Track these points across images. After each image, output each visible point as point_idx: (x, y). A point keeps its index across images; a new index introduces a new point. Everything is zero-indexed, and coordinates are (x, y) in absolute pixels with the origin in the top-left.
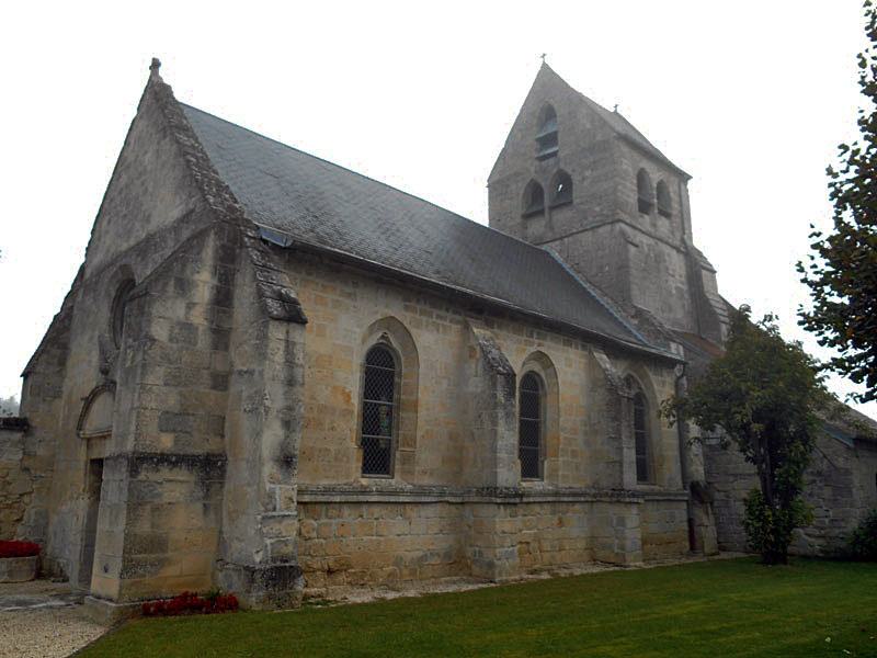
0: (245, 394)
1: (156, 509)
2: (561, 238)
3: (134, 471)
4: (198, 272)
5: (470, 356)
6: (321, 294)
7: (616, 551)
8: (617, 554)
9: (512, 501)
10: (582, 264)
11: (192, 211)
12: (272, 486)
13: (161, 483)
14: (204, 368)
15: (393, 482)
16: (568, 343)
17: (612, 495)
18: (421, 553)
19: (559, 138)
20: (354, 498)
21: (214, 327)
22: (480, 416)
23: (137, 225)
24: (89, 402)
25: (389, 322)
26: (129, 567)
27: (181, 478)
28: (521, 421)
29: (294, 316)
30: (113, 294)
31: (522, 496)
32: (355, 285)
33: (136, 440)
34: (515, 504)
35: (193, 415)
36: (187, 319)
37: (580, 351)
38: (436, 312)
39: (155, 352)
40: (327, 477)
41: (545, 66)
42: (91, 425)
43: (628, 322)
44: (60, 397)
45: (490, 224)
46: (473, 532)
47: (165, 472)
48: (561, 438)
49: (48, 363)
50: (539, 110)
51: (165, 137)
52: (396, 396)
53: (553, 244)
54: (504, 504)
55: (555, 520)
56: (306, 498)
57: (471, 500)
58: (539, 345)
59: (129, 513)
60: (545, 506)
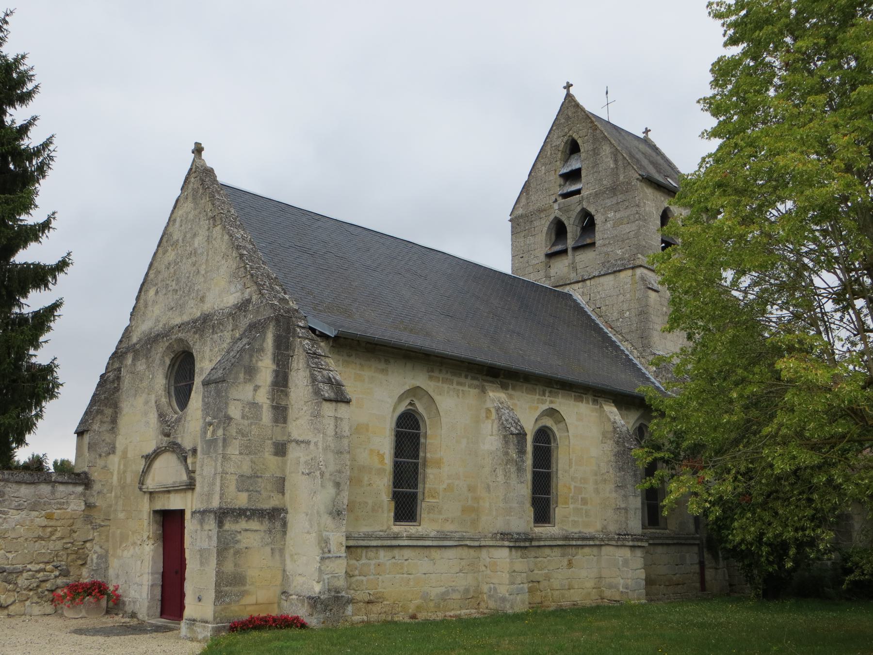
0: (302, 460)
1: (237, 553)
2: (584, 281)
3: (220, 524)
5: (487, 417)
6: (358, 372)
7: (621, 589)
9: (522, 544)
11: (249, 301)
13: (240, 532)
14: (268, 439)
15: (420, 528)
16: (579, 399)
18: (443, 589)
19: (583, 175)
20: (389, 543)
21: (274, 404)
23: (191, 303)
25: (415, 391)
28: (534, 472)
29: (341, 398)
31: (531, 540)
32: (387, 362)
33: (221, 498)
34: (526, 547)
35: (261, 477)
36: (254, 399)
37: (591, 406)
38: (455, 379)
39: (233, 430)
41: (569, 97)
42: (153, 480)
44: (114, 452)
45: (518, 254)
47: (243, 524)
48: (572, 487)
49: (102, 422)
51: (215, 226)
52: (421, 454)
53: (576, 286)
57: (487, 543)
58: (551, 402)
60: (555, 549)
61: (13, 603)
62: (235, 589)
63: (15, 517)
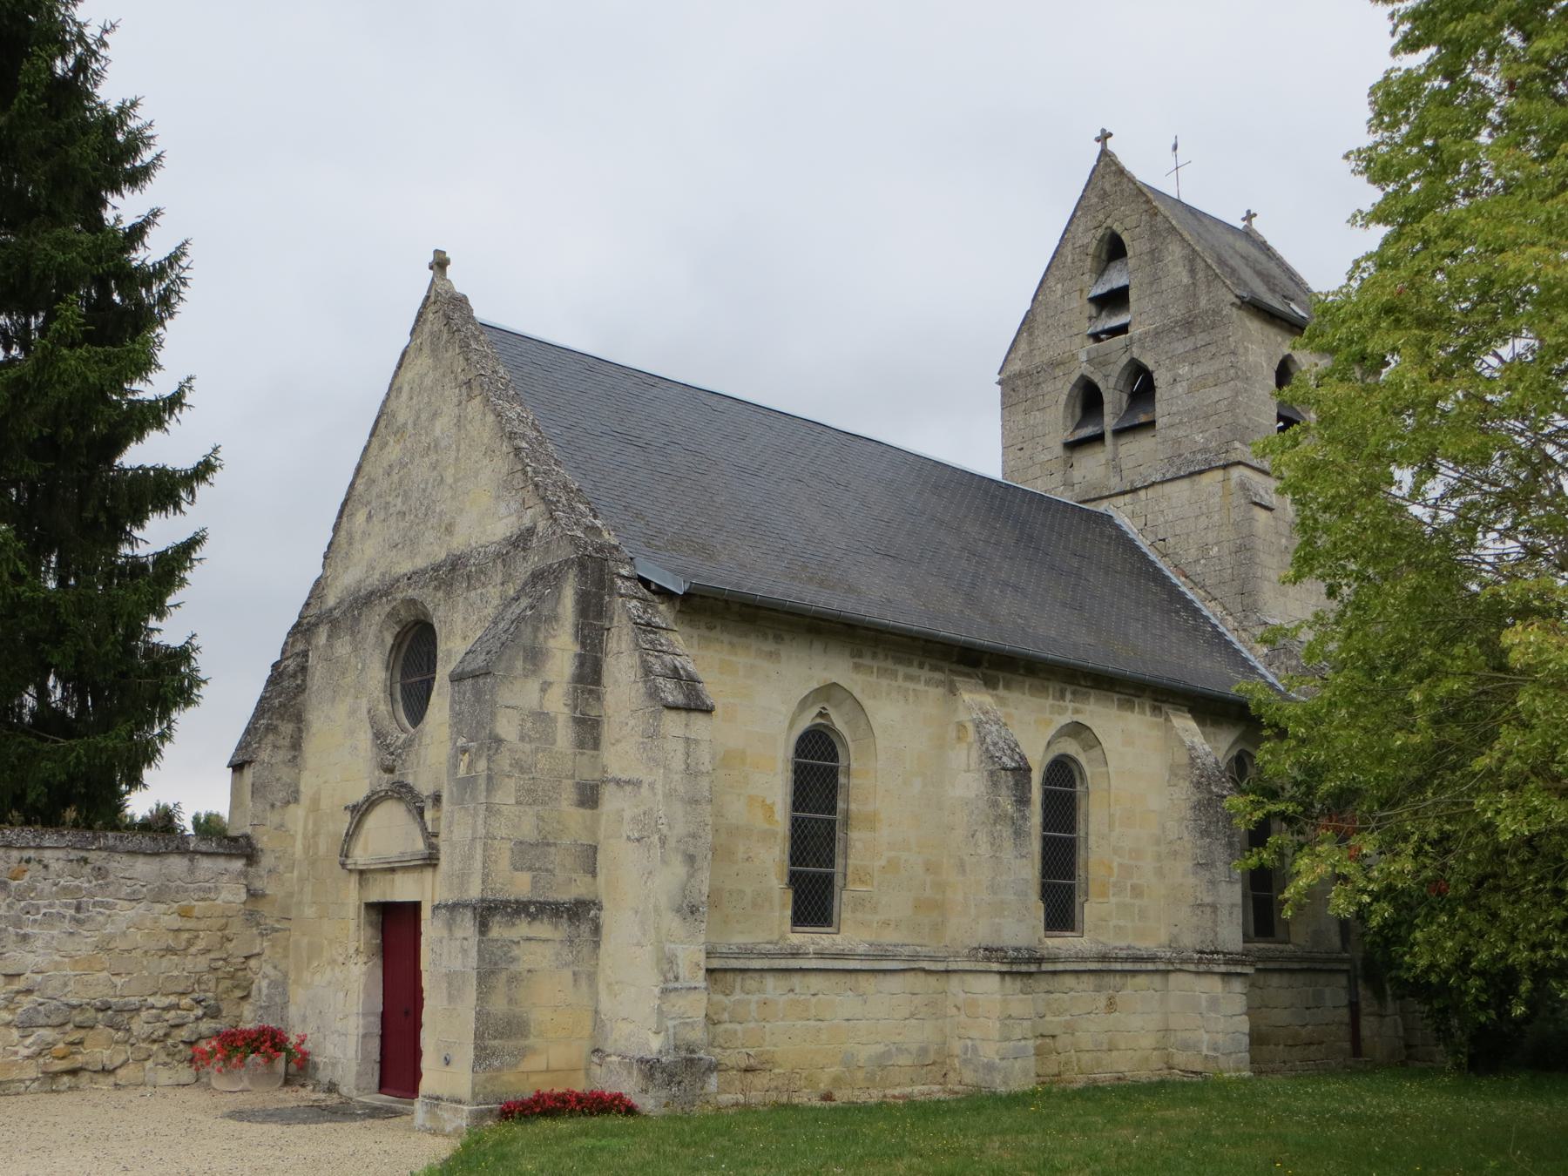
0: (627, 815)
1: (513, 979)
2: (1134, 491)
4: (554, 637)
5: (959, 738)
7: (1205, 1052)
8: (1206, 1056)
9: (1024, 968)
10: (1171, 541)
12: (673, 946)
14: (567, 777)
15: (838, 938)
16: (1126, 704)
17: (1200, 961)
18: (881, 1048)
20: (783, 964)
21: (578, 715)
22: (973, 836)
23: (430, 536)
24: (360, 812)
25: (829, 691)
26: (482, 1055)
27: (544, 936)
30: (389, 640)
31: (1040, 961)
32: (778, 638)
35: (555, 844)
38: (902, 670)
39: (504, 761)
40: (742, 933)
42: (365, 850)
43: (1251, 649)
44: (296, 800)
45: (1004, 475)
46: (963, 1018)
47: (523, 928)
50: (1095, 242)
51: (470, 398)
52: (841, 805)
53: (1120, 501)
54: (1010, 973)
55: (1102, 1001)
56: (715, 964)
58: (1076, 711)
59: (479, 984)
60: (1085, 978)
61: (125, 1063)
62: (510, 1044)
63: (126, 913)
